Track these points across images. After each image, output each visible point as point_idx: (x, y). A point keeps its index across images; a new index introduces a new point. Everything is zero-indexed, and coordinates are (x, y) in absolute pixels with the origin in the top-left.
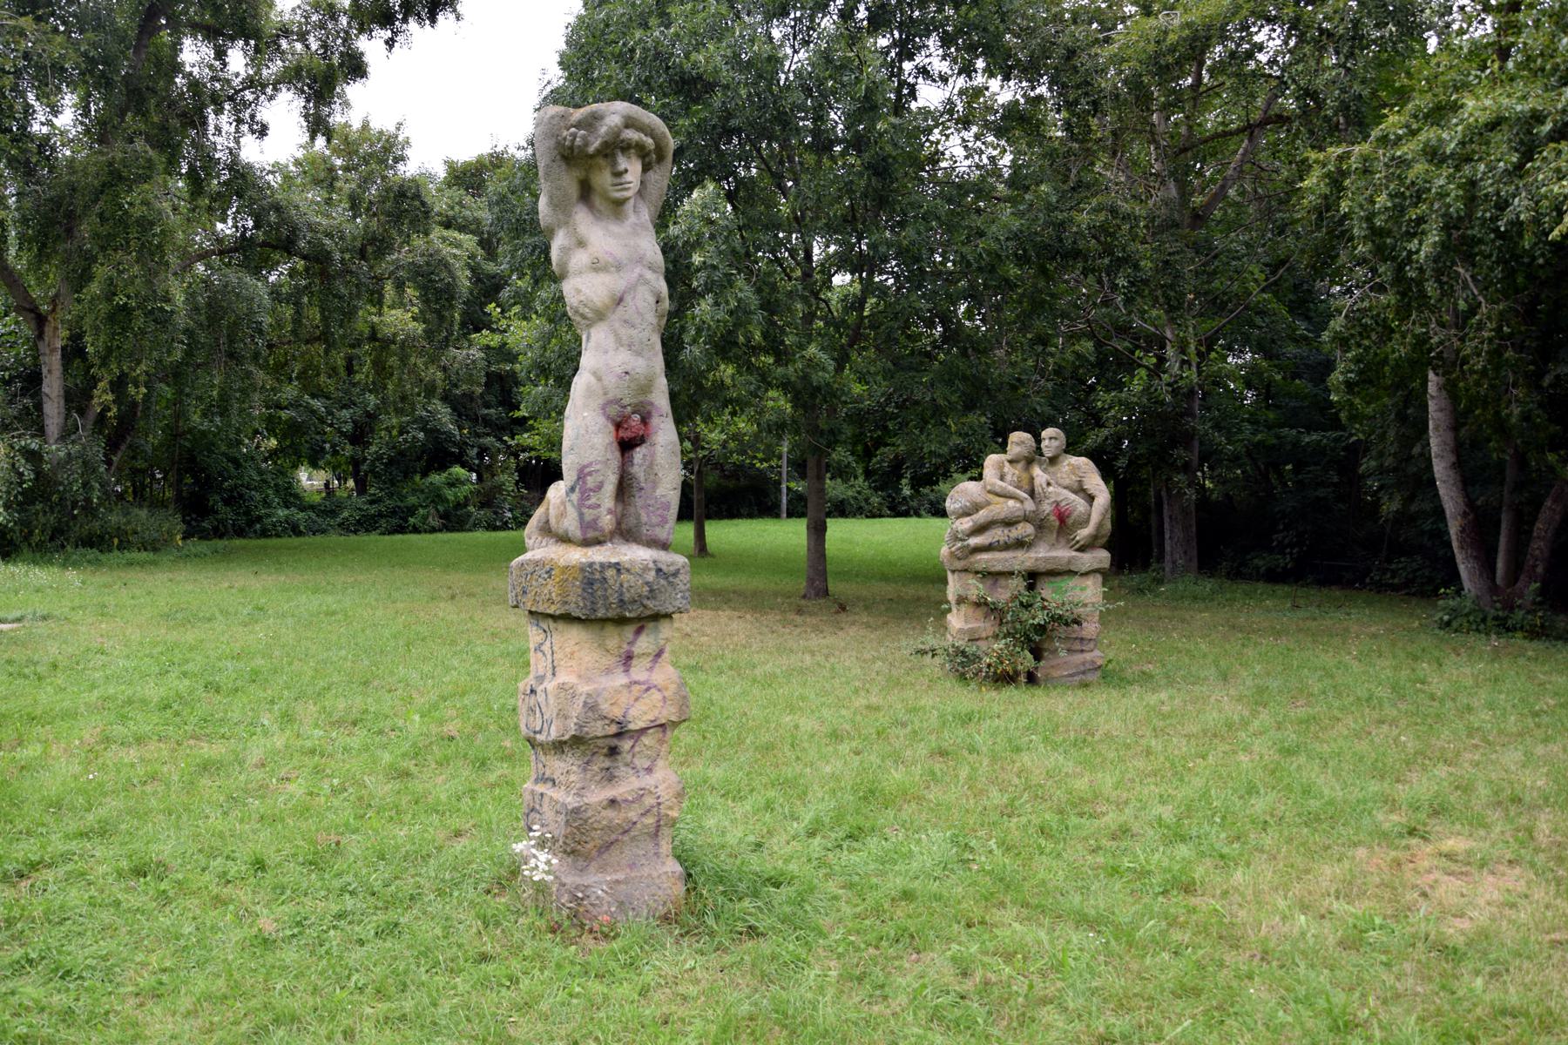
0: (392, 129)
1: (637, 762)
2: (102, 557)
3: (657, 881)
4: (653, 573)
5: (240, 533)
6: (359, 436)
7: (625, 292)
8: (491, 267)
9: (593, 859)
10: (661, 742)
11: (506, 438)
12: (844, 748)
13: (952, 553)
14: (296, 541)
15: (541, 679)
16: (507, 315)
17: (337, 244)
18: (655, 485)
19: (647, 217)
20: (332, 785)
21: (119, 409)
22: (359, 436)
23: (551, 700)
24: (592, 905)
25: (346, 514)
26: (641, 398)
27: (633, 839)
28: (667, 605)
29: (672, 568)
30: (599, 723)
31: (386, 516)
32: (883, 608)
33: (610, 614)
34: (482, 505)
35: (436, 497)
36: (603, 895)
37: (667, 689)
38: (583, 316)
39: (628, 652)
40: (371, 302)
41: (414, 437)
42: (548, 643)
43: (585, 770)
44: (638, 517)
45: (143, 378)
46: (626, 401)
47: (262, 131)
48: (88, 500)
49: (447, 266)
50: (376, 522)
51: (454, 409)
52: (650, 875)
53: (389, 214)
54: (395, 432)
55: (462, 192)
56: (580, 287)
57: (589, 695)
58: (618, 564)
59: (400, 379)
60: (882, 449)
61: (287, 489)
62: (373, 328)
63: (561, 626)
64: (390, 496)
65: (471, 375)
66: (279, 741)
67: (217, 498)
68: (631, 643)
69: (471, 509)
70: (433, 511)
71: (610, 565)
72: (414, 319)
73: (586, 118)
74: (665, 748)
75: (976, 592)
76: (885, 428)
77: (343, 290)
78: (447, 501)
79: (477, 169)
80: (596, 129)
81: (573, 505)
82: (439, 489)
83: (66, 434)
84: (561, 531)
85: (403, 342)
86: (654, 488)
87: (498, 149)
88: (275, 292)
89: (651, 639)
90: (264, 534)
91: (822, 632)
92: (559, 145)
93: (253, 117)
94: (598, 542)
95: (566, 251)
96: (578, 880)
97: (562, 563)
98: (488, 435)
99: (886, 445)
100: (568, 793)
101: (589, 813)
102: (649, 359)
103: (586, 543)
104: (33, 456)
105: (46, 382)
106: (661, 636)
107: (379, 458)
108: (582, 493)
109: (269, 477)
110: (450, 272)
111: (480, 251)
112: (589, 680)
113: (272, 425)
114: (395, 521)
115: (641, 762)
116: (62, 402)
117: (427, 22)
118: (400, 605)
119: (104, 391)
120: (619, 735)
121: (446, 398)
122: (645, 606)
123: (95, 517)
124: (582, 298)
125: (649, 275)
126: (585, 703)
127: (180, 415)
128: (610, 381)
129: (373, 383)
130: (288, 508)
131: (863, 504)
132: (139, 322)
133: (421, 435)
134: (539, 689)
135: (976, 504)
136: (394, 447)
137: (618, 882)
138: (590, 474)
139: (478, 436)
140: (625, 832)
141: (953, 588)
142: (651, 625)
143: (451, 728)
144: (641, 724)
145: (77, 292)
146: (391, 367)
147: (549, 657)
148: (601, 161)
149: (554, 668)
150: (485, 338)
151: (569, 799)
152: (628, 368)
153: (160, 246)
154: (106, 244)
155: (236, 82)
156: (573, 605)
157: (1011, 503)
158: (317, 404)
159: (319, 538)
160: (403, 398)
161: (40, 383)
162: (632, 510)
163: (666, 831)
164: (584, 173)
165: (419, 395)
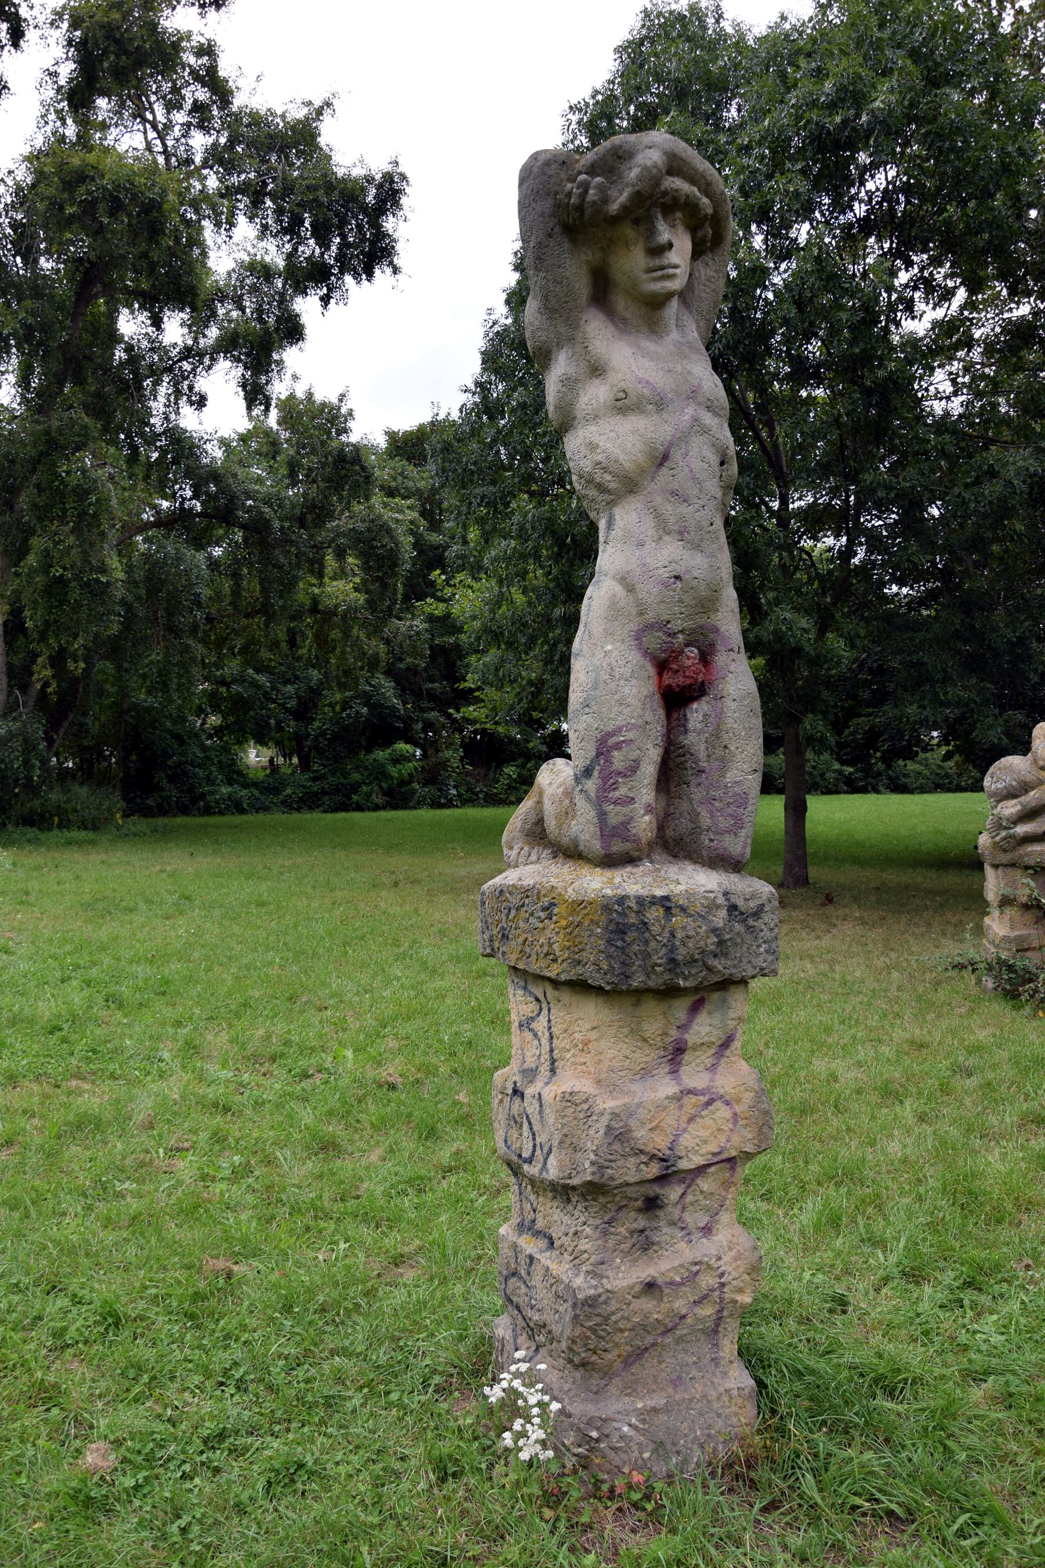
0: (335, 401)
1: (689, 1218)
2: (43, 836)
4: (723, 913)
5: (184, 811)
6: (304, 711)
7: (671, 444)
8: (435, 538)
9: (615, 1375)
10: (727, 1184)
11: (451, 711)
12: (908, 1111)
13: (995, 843)
14: (237, 819)
15: (531, 1074)
16: (452, 582)
17: (276, 512)
18: (724, 764)
19: (696, 334)
20: (232, 1164)
21: (58, 686)
22: (304, 711)
23: (551, 1118)
25: (288, 791)
26: (701, 620)
27: (679, 1340)
28: (745, 965)
29: (752, 904)
30: (633, 1160)
31: (329, 793)
32: (872, 898)
35: (380, 773)
36: (632, 1433)
37: (739, 1100)
38: (602, 488)
40: (312, 572)
41: (357, 712)
42: (543, 1020)
43: (605, 1234)
44: (695, 817)
46: (677, 625)
47: (200, 402)
48: (29, 778)
49: (389, 531)
51: (398, 683)
53: (329, 480)
54: (338, 708)
55: (404, 462)
56: (596, 439)
57: (615, 1115)
58: (666, 898)
59: (343, 652)
60: (856, 720)
61: (230, 766)
62: (315, 601)
63: (566, 996)
64: (333, 772)
65: (414, 647)
66: (173, 1089)
67: (162, 774)
68: (683, 1027)
70: (376, 788)
71: (654, 901)
72: (356, 589)
73: (603, 158)
75: (1027, 891)
76: (855, 697)
77: (282, 560)
78: (391, 778)
79: (418, 439)
80: (620, 176)
81: (588, 799)
82: (383, 765)
84: (565, 841)
85: (345, 613)
87: (440, 417)
88: (214, 564)
90: (208, 811)
91: (813, 930)
92: (560, 207)
93: (191, 388)
94: (629, 860)
95: (570, 384)
96: (592, 1410)
97: (571, 894)
98: (432, 709)
99: (859, 716)
100: (577, 1267)
101: (613, 1306)
102: (712, 555)
103: (610, 861)
106: (732, 1014)
107: (323, 734)
108: (604, 779)
109: (212, 754)
110: (392, 537)
111: (423, 522)
113: (214, 701)
114: (338, 798)
115: (695, 1219)
117: (364, 276)
118: (339, 894)
119: (44, 667)
120: (661, 1179)
121: (388, 673)
122: (710, 969)
124: (599, 458)
125: (708, 419)
126: (609, 1128)
127: (123, 693)
128: (649, 592)
129: (316, 656)
130: (231, 784)
131: (818, 779)
132: (75, 594)
133: (365, 710)
134: (530, 1091)
135: (1025, 783)
136: (337, 723)
137: (655, 1410)
138: (618, 746)
139: (422, 710)
141: (993, 884)
142: (716, 996)
143: (391, 1070)
144: (698, 1160)
145: (16, 565)
146: (333, 640)
147: (545, 1041)
148: (628, 231)
149: (553, 1061)
150: (431, 606)
151: (579, 1281)
152: (680, 569)
153: (95, 515)
154: (43, 513)
155: (174, 352)
158: (262, 679)
159: (261, 817)
160: (346, 673)
162: (685, 805)
165: (362, 669)
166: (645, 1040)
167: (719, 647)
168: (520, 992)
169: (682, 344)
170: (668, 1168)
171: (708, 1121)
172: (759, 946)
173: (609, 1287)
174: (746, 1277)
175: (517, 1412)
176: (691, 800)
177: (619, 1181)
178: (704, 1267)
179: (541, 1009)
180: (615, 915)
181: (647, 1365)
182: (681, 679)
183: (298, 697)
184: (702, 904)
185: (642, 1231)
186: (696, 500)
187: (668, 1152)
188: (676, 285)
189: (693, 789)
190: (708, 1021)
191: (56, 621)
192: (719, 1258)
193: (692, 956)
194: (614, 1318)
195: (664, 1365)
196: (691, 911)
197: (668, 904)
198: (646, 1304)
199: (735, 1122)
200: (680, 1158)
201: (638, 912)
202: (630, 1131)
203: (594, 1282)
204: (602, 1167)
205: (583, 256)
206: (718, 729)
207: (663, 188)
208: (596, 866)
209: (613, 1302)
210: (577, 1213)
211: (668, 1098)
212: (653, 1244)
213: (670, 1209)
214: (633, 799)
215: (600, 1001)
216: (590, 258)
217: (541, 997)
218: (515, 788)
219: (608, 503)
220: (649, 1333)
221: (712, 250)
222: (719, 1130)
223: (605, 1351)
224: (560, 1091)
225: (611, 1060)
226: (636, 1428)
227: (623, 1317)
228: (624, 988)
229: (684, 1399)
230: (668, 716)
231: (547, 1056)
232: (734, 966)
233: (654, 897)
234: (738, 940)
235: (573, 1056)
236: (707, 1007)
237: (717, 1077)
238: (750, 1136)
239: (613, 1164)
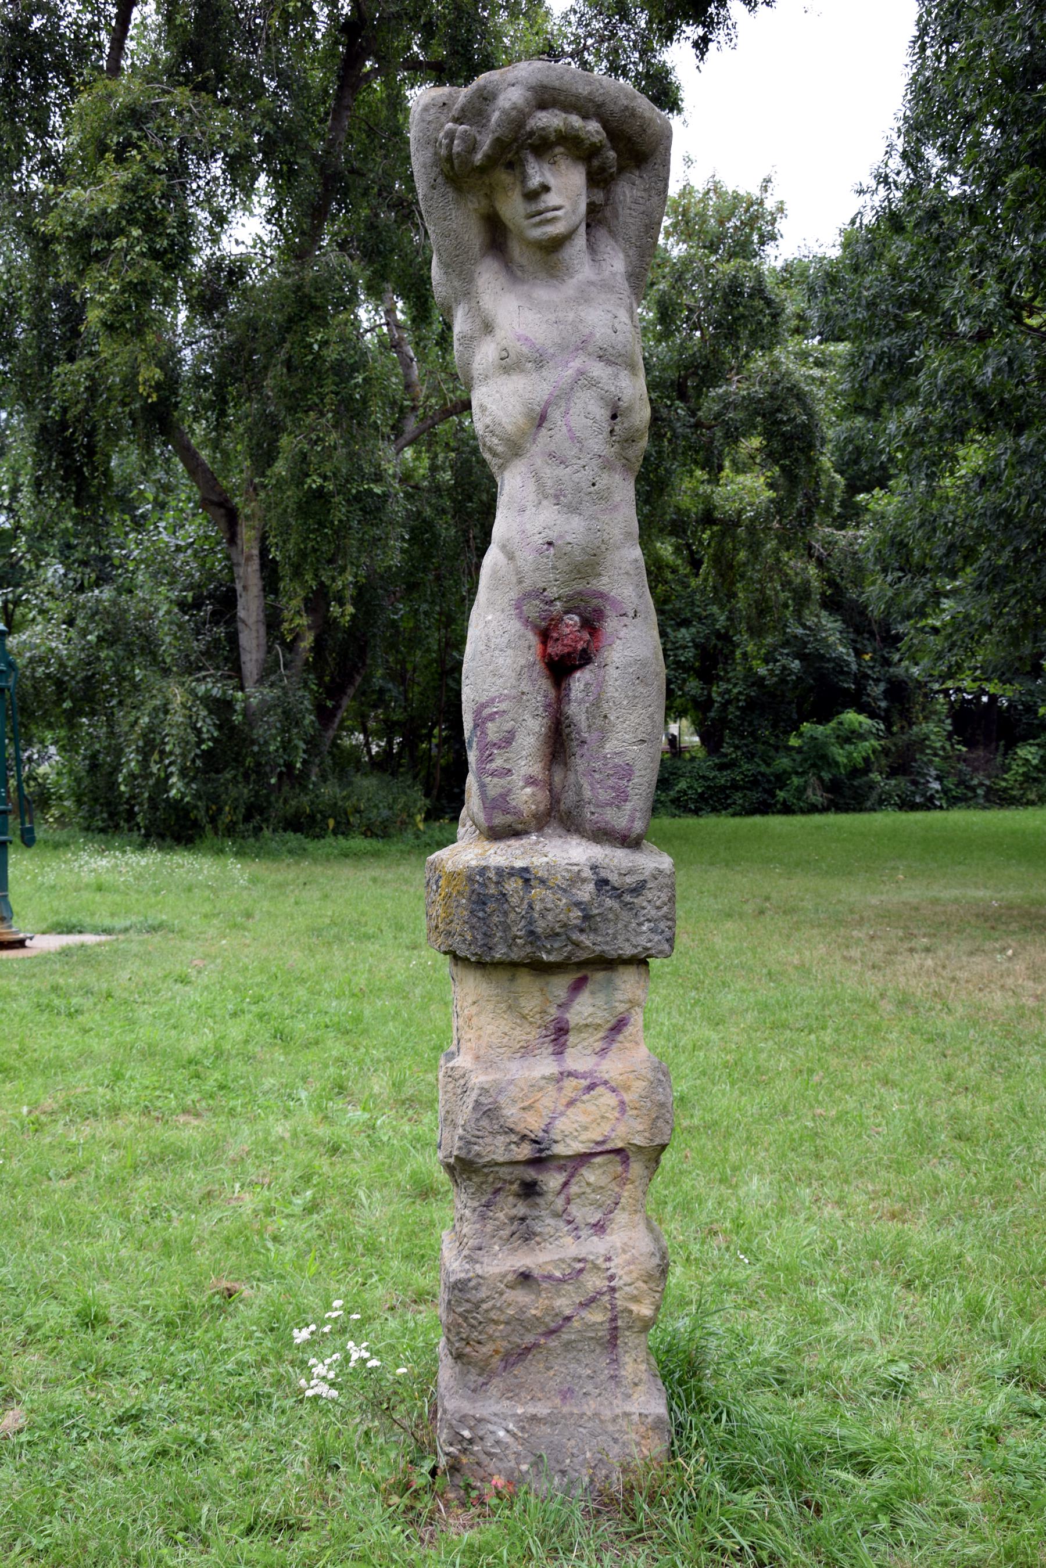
0: (756, 193)
2: (311, 845)
3: (611, 1428)
4: (591, 887)
7: (548, 404)
9: (492, 1374)
10: (621, 1180)
24: (488, 1454)
25: (683, 785)
27: (568, 1346)
28: (620, 941)
29: (628, 880)
30: (501, 1140)
33: (515, 955)
34: (893, 772)
36: (509, 1439)
37: (627, 1088)
39: (558, 1020)
41: (784, 668)
43: (483, 1217)
45: (349, 592)
46: (552, 592)
48: (290, 766)
49: (800, 397)
50: (728, 797)
52: (596, 1415)
57: (484, 1091)
58: (526, 870)
64: (750, 757)
69: (875, 776)
70: (813, 780)
74: (627, 1193)
78: (837, 764)
83: (268, 671)
85: (753, 520)
86: (603, 740)
89: (600, 999)
104: (221, 707)
105: (241, 603)
106: (619, 995)
112: (490, 1065)
114: (755, 795)
116: (263, 630)
119: (298, 613)
120: (538, 1162)
122: (577, 944)
123: (304, 788)
132: (339, 512)
133: (796, 665)
137: (534, 1418)
138: (491, 718)
140: (551, 1332)
142: (600, 976)
144: (576, 1147)
148: (504, 177)
152: (552, 535)
161: (235, 607)
162: (572, 778)
163: (628, 1338)
164: (484, 202)
166: (524, 1017)
167: (609, 613)
172: (640, 924)
173: (480, 1272)
174: (640, 1284)
175: (521, 1481)
177: (488, 1159)
178: (589, 1266)
183: (696, 646)
184: (563, 877)
185: (523, 1219)
190: (591, 1001)
191: (314, 550)
193: (552, 929)
194: (485, 1306)
195: (552, 1373)
197: (527, 876)
198: (521, 1297)
199: (623, 1111)
200: (556, 1142)
201: (497, 883)
202: (500, 1108)
203: (467, 1266)
204: (469, 1143)
206: (598, 698)
209: (484, 1288)
211: (544, 1078)
212: (535, 1234)
213: (550, 1197)
214: (509, 771)
215: (479, 973)
218: (1036, 780)
220: (528, 1331)
222: (603, 1117)
223: (479, 1343)
225: (489, 1036)
226: (514, 1435)
227: (494, 1307)
228: (488, 959)
229: (572, 1414)
233: (513, 868)
234: (611, 916)
236: (589, 987)
237: (604, 1062)
238: (640, 1128)
239: (480, 1141)
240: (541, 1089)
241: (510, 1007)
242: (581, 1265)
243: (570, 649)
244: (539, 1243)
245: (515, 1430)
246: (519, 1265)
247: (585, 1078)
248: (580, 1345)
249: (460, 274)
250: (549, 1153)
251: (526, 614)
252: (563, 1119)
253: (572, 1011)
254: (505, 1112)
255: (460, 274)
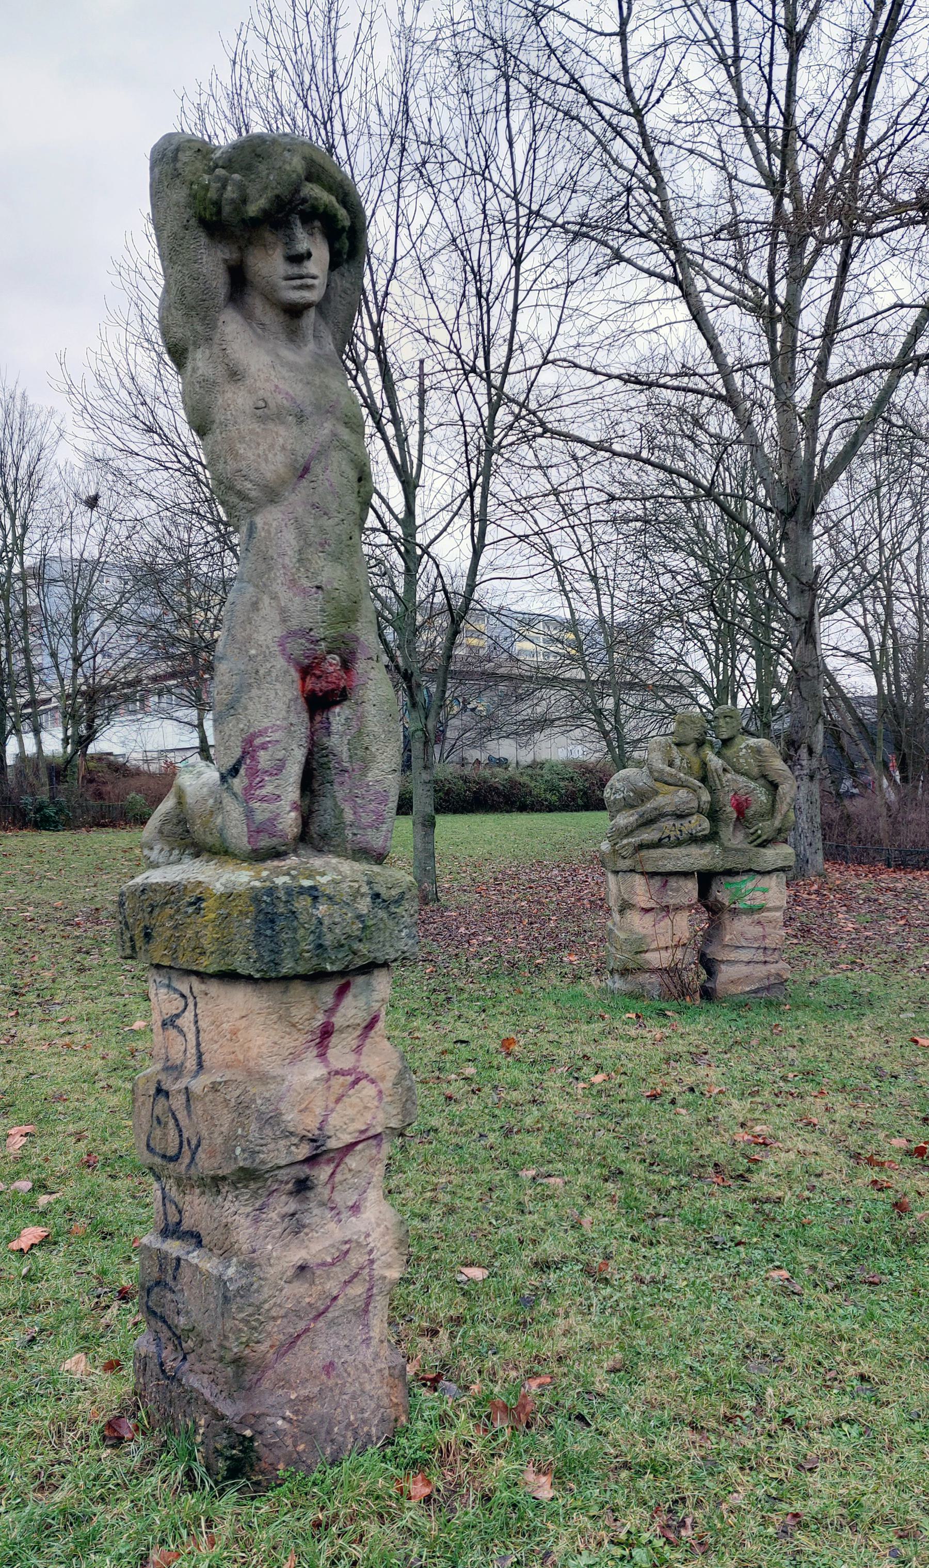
7: (312, 458)
19: (332, 347)
26: (343, 629)
27: (332, 1323)
29: (393, 892)
37: (383, 1078)
42: (189, 1015)
43: (256, 1221)
44: (339, 814)
46: (317, 634)
58: (313, 888)
68: (331, 1011)
71: (302, 891)
86: (365, 769)
94: (277, 854)
103: (258, 856)
120: (311, 1160)
137: (308, 1399)
142: (360, 980)
144: (347, 1139)
156: (240, 957)
157: (683, 793)
166: (294, 1025)
167: (359, 656)
168: (163, 991)
169: (319, 355)
170: (318, 1147)
171: (354, 1100)
172: (400, 931)
174: (394, 1251)
176: (334, 797)
178: (354, 1245)
179: (186, 1005)
180: (263, 905)
181: (300, 1354)
182: (324, 684)
185: (293, 1215)
186: (336, 514)
187: (317, 1132)
188: (313, 296)
189: (336, 787)
190: (354, 1004)
192: (368, 1235)
193: (339, 941)
194: (266, 1306)
195: (317, 1352)
196: (337, 899)
197: (316, 893)
198: (299, 1288)
199: (381, 1099)
200: (329, 1137)
205: (219, 253)
207: (302, 194)
208: (244, 861)
210: (227, 1204)
211: (316, 1080)
212: (304, 1226)
213: (319, 1189)
216: (227, 256)
217: (186, 992)
219: (249, 511)
220: (301, 1319)
221: (347, 261)
222: (366, 1107)
223: (258, 1342)
224: (208, 1082)
225: (259, 1047)
226: (290, 1421)
230: (312, 719)
231: (194, 1051)
232: (378, 950)
234: (382, 926)
235: (221, 1046)
236: (353, 990)
238: (395, 1112)
239: (264, 1149)
240: (313, 1090)
241: (280, 1018)
242: (348, 1246)
243: (334, 686)
244: (307, 1234)
245: (291, 1416)
246: (296, 1259)
247: (351, 1074)
248: (340, 1320)
249: (205, 318)
250: (324, 1148)
251: (289, 651)
252: (334, 1115)
253: (338, 1014)
254: (285, 1117)
255: (205, 318)
